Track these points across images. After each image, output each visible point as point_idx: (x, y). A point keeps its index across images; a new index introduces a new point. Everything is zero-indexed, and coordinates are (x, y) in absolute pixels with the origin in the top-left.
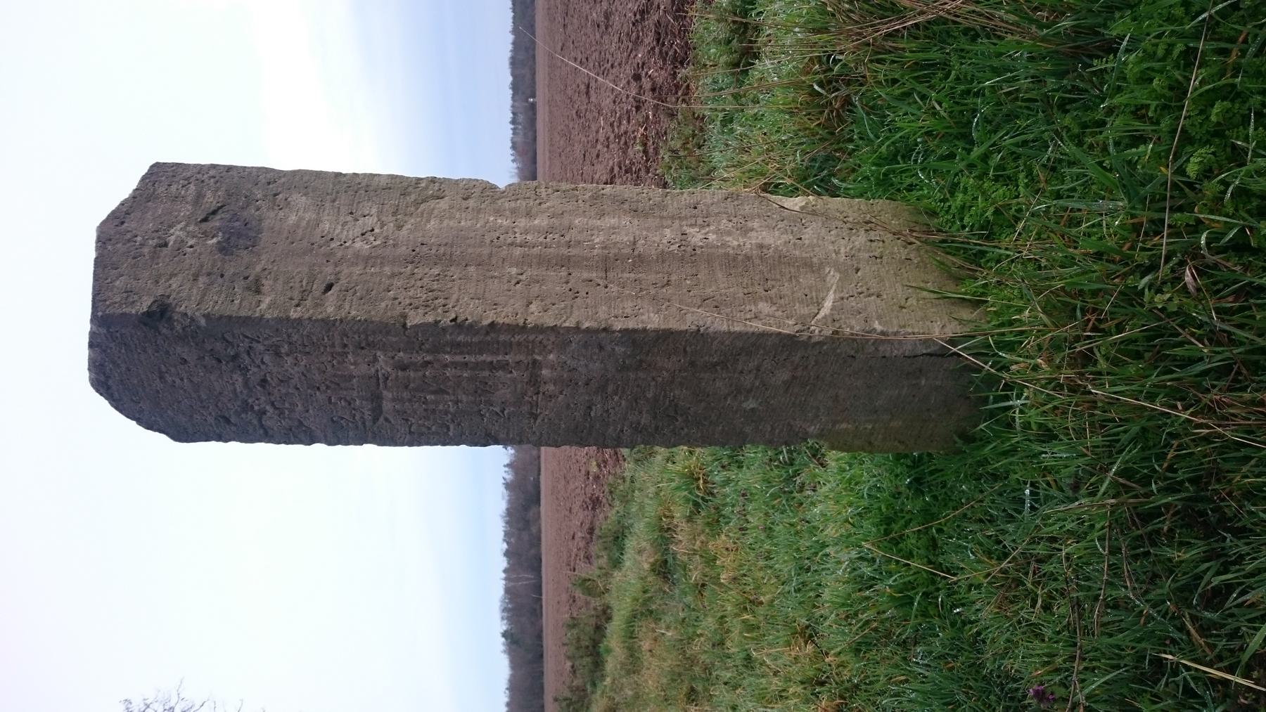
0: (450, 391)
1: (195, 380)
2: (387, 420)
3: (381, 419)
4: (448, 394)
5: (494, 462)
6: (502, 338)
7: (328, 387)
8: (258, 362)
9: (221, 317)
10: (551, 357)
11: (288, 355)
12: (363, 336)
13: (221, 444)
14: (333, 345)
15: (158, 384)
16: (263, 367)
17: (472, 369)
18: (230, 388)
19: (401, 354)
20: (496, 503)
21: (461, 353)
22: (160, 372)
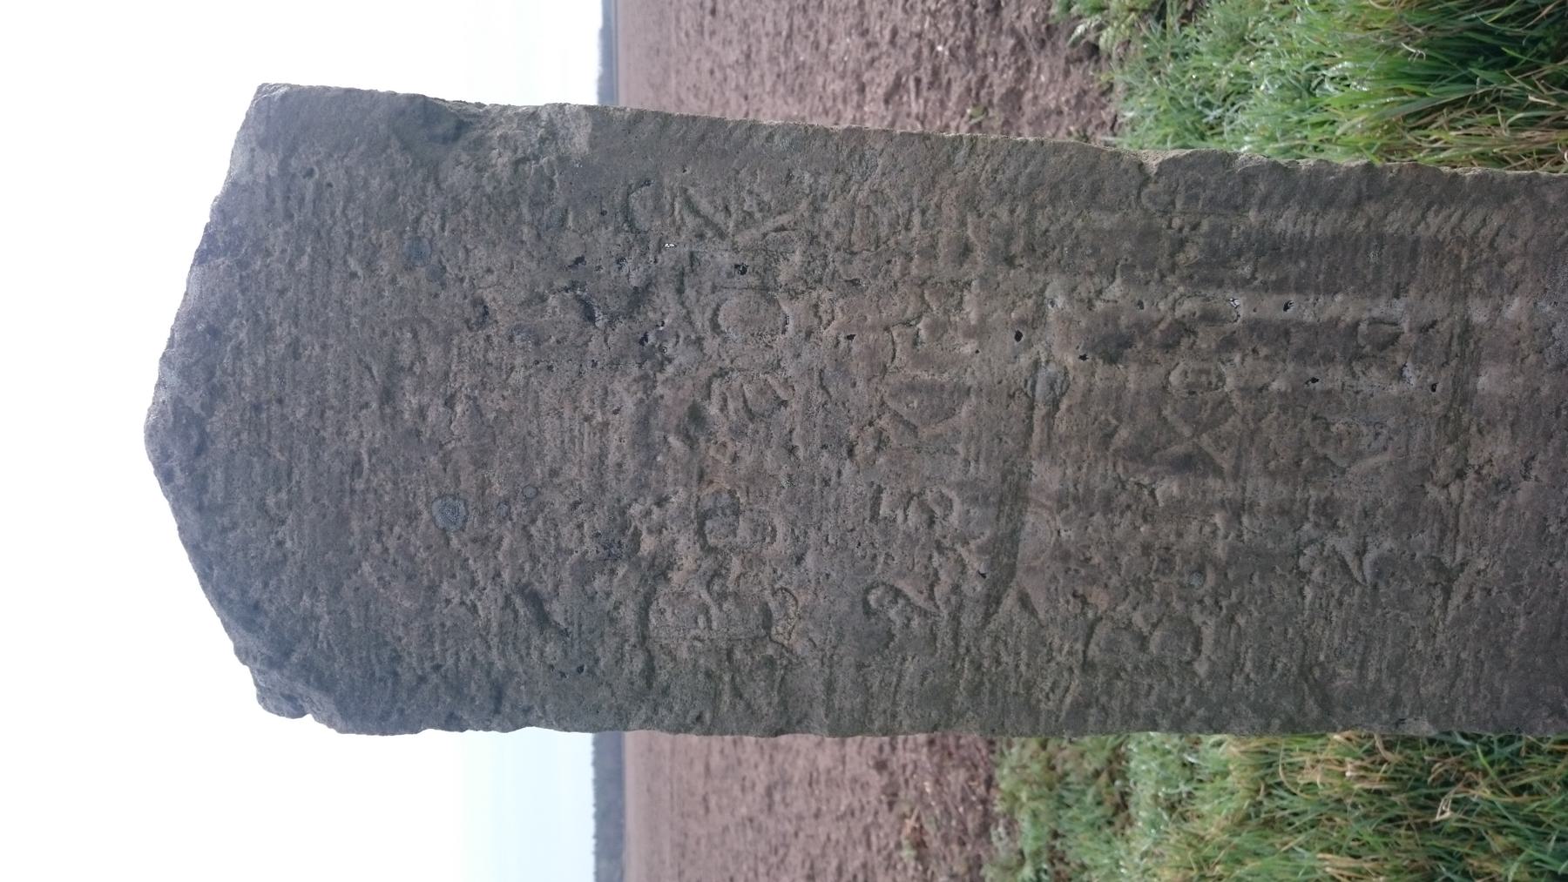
0: (1225, 461)
1: (494, 403)
2: (1024, 601)
3: (1009, 602)
4: (1218, 472)
5: (587, 738)
6: (1395, 223)
7: (881, 443)
8: (701, 321)
9: (639, 116)
10: (1515, 307)
11: (793, 295)
12: (1021, 211)
13: (195, 239)
14: (929, 253)
15: (366, 432)
16: (711, 344)
17: (1301, 356)
18: (589, 448)
19: (1116, 290)
20: (587, 774)
21: (1280, 286)
22: (394, 369)
